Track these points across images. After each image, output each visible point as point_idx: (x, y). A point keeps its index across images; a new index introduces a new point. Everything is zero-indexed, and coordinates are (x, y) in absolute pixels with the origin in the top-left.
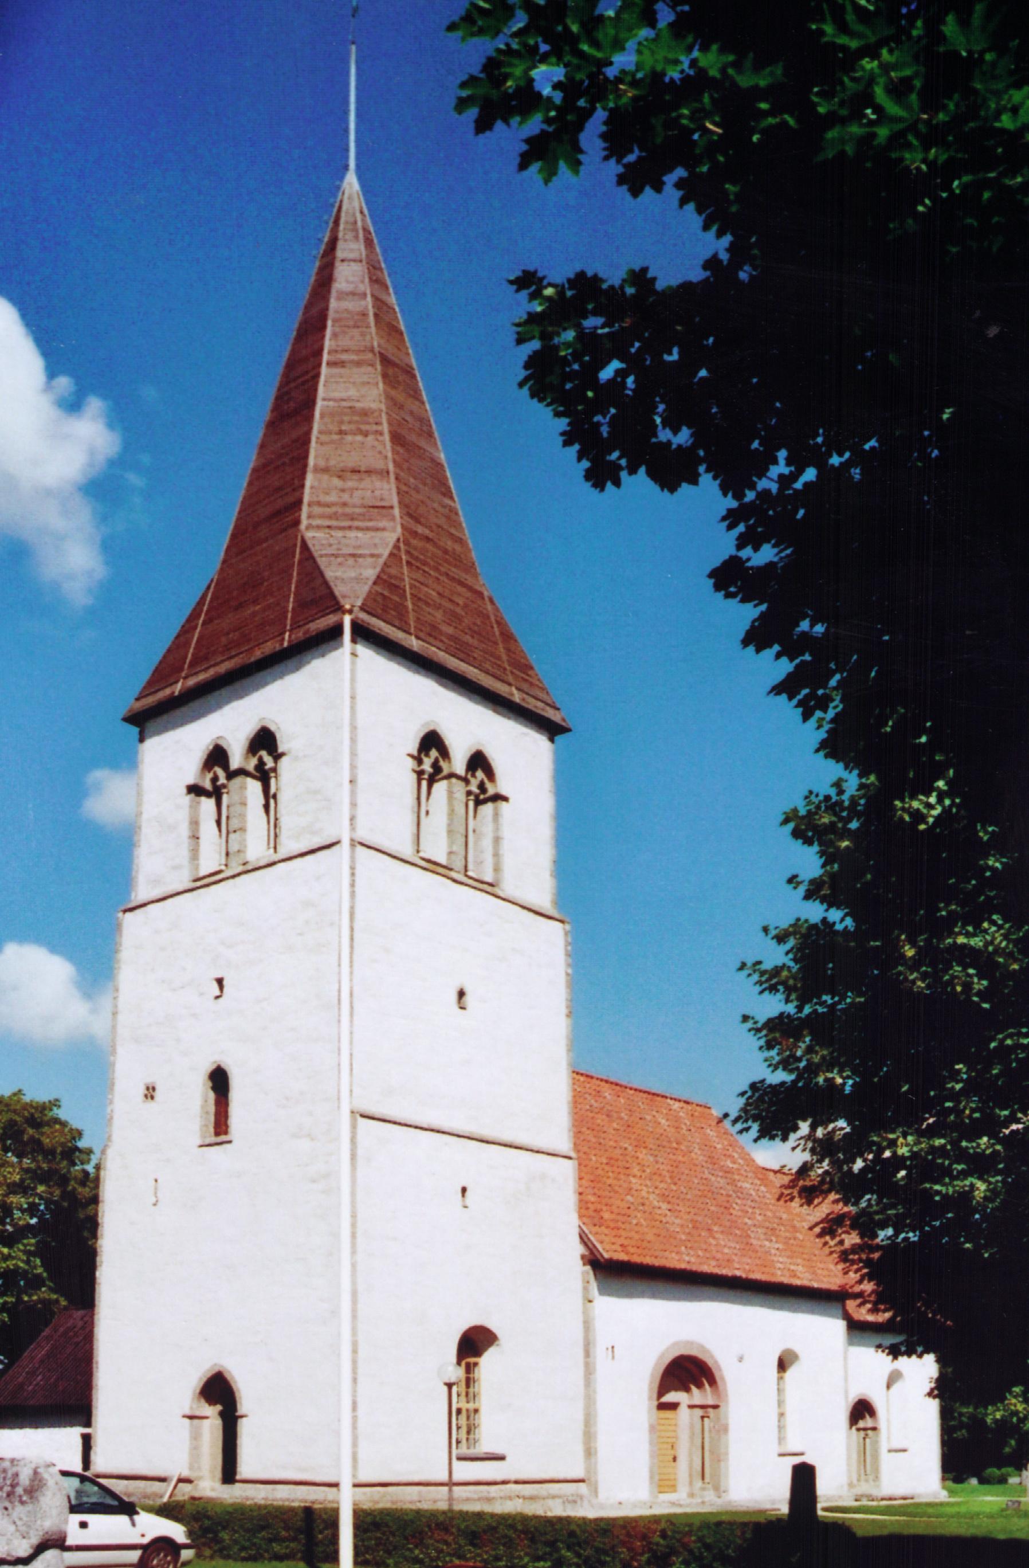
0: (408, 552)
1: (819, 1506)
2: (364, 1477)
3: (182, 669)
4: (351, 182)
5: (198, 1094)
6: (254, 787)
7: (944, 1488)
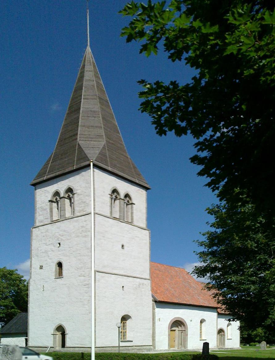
0: (108, 147)
1: (210, 350)
2: (97, 346)
3: (46, 173)
4: (89, 49)
5: (54, 267)
6: (67, 201)
7: (240, 347)
